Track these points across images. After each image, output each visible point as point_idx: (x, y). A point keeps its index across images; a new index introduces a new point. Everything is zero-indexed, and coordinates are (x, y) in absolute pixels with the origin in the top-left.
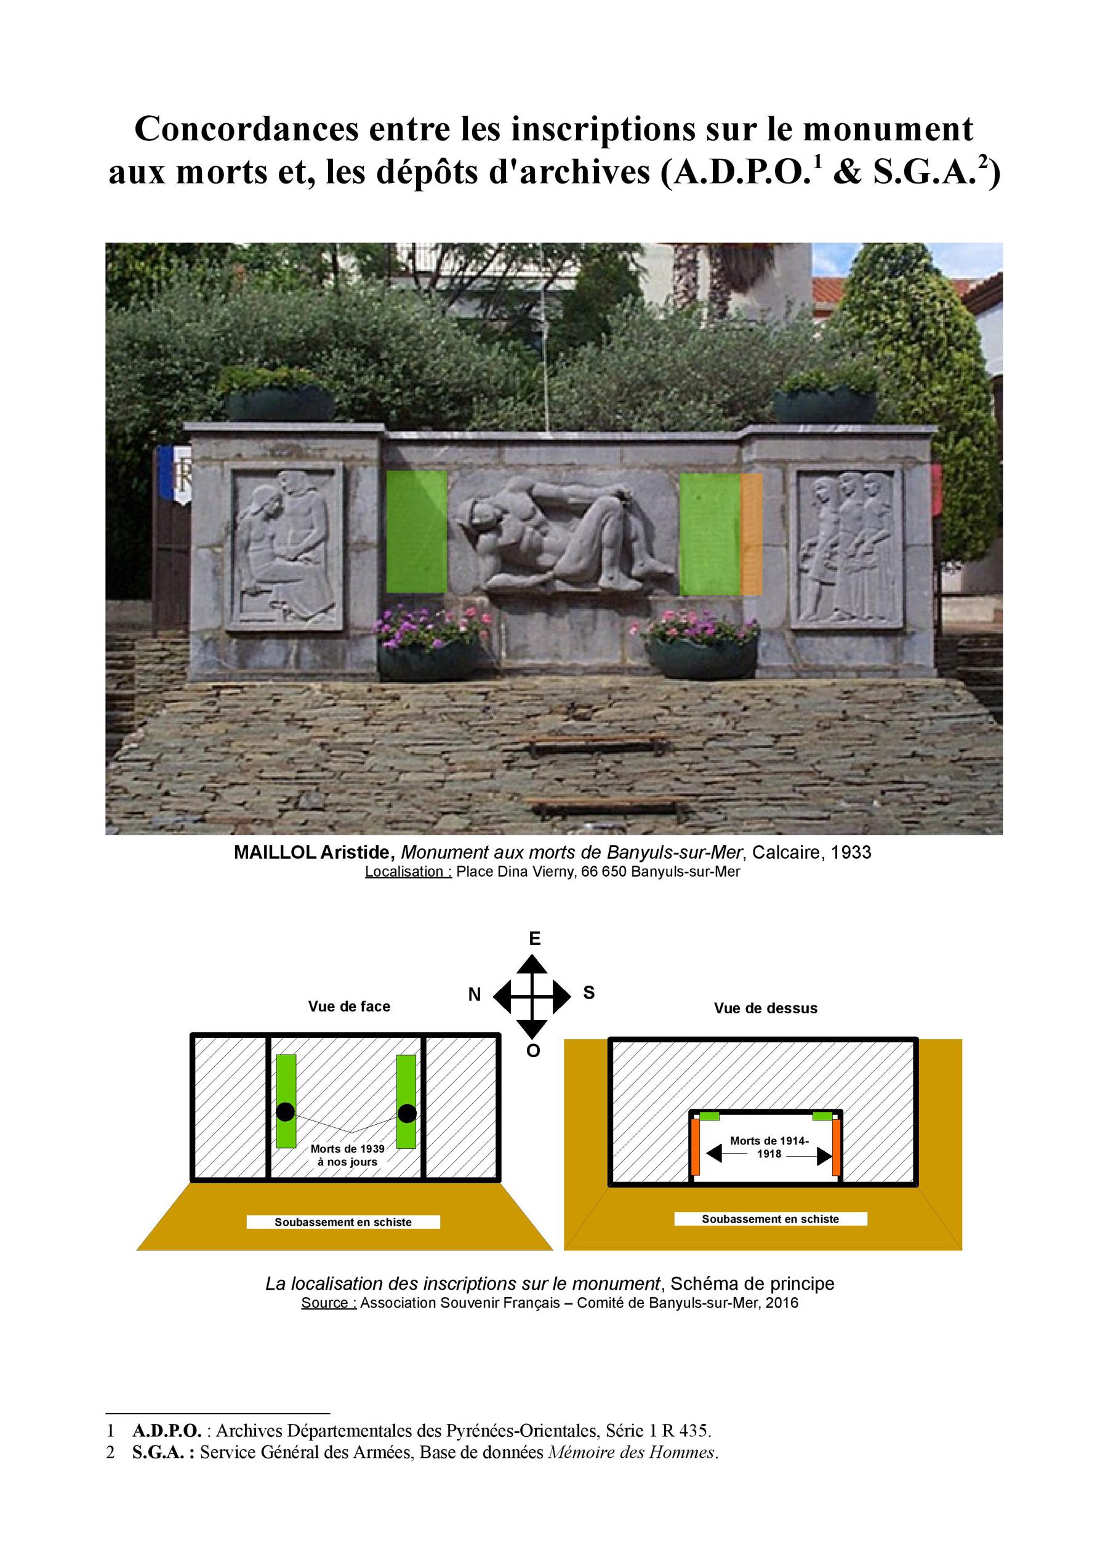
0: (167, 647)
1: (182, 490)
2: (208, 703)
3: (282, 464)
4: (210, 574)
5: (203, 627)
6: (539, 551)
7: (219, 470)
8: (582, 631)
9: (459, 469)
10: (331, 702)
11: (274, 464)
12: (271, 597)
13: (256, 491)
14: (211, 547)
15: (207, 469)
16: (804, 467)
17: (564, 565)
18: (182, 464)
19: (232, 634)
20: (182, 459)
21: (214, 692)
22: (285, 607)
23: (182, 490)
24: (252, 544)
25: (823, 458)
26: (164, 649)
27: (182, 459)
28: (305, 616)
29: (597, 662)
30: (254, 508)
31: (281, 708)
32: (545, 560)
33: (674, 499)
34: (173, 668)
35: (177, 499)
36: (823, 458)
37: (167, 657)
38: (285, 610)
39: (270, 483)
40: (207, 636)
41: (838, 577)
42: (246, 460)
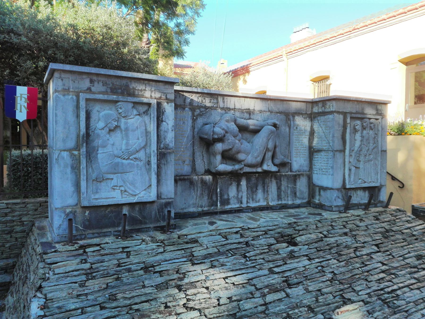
0: (9, 206)
1: (21, 112)
2: (81, 262)
3: (121, 98)
4: (69, 170)
5: (66, 204)
6: (239, 152)
7: (75, 97)
8: (252, 190)
9: (199, 109)
10: (161, 250)
11: (114, 97)
12: (114, 183)
13: (102, 114)
14: (70, 150)
15: (67, 97)
16: (354, 115)
17: (250, 159)
18: (21, 97)
19: (85, 208)
20: (21, 95)
21: (81, 251)
22: (123, 189)
23: (21, 112)
24: (100, 149)
25: (357, 112)
26: (8, 208)
27: (21, 95)
28: (134, 194)
29: (257, 204)
30: (101, 124)
31: (134, 259)
32: (241, 156)
33: (287, 130)
34: (15, 219)
35: (17, 118)
36: (357, 112)
37: (10, 212)
38: (121, 191)
39: (111, 109)
40: (68, 211)
41: (361, 165)
42: (94, 93)
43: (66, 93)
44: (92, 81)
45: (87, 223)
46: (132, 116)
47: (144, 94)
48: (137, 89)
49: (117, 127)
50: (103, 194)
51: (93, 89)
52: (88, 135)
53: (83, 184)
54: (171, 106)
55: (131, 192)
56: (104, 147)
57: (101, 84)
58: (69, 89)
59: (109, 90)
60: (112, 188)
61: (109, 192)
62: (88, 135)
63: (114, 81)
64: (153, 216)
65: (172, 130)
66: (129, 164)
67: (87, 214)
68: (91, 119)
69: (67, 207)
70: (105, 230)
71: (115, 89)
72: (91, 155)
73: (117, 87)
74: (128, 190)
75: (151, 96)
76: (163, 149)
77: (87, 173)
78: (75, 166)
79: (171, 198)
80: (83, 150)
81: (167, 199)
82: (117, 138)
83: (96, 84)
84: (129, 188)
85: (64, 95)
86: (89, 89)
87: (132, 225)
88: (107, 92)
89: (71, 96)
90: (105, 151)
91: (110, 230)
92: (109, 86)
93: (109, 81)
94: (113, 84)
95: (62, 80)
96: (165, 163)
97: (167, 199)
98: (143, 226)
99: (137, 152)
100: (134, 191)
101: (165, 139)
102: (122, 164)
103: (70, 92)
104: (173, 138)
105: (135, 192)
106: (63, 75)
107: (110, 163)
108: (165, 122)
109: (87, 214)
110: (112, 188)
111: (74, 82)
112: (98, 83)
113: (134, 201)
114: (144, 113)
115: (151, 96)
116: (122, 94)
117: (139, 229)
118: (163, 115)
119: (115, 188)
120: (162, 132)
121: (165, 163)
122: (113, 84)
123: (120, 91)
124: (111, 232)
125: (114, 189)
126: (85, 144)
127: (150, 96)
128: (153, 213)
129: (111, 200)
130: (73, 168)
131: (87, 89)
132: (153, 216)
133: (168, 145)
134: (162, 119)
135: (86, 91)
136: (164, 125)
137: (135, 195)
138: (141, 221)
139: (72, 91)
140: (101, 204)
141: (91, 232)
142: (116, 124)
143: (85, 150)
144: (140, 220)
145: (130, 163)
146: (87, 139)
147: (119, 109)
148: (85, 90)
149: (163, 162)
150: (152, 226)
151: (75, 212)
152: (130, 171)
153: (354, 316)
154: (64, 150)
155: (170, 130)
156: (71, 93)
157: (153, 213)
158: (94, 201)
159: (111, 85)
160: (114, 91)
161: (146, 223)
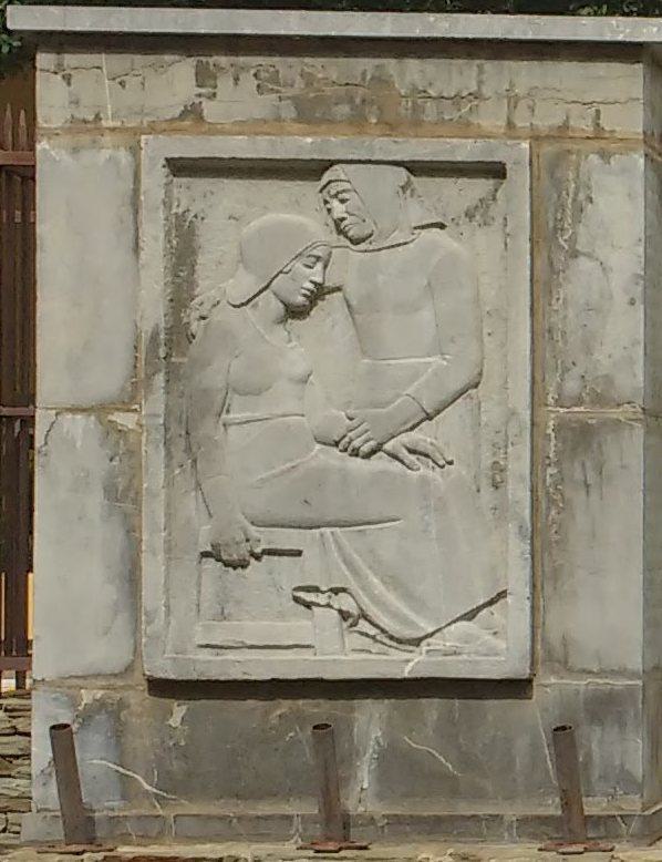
3: (335, 144)
4: (95, 501)
7: (124, 157)
11: (303, 145)
14: (100, 409)
15: (87, 156)
24: (235, 400)
30: (242, 284)
39: (296, 206)
40: (87, 697)
42: (214, 130)
43: (86, 139)
44: (203, 77)
45: (176, 766)
46: (398, 237)
47: (474, 120)
48: (432, 92)
49: (319, 293)
50: (252, 628)
51: (210, 110)
52: (177, 335)
53: (153, 570)
54: (624, 170)
55: (385, 622)
56: (254, 391)
57: (249, 82)
58: (98, 118)
59: (289, 112)
60: (296, 600)
61: (281, 616)
62: (177, 335)
63: (318, 66)
64: (520, 761)
65: (632, 302)
66: (379, 478)
67: (175, 721)
68: (201, 260)
69: (84, 677)
70: (264, 809)
71: (320, 100)
72: (188, 435)
73: (329, 91)
74: (373, 611)
75: (510, 124)
76: (579, 401)
77: (168, 515)
78: (121, 482)
79: (622, 673)
80: (155, 402)
81: (601, 673)
82: (316, 349)
83: (224, 85)
84: (376, 600)
85: (75, 150)
86: (193, 112)
87: (406, 795)
88: (278, 119)
89: (106, 154)
90: (257, 415)
91: (287, 809)
92: (290, 92)
93: (289, 67)
94: (309, 80)
95: (68, 79)
96: (592, 478)
97: (601, 673)
98: (464, 809)
99: (429, 417)
100: (412, 624)
101: (588, 351)
102: (345, 476)
103: (101, 131)
104: (635, 343)
105: (418, 628)
106: (70, 59)
107: (283, 473)
108: (589, 256)
109: (175, 721)
110: (296, 600)
111: (122, 84)
112: (236, 79)
113: (406, 672)
114: (470, 215)
115: (510, 124)
116: (357, 122)
117: (438, 820)
118: (577, 220)
119: (310, 597)
120: (571, 313)
121: (592, 478)
122: (309, 80)
123: (344, 109)
124: (289, 818)
125: (308, 605)
126: (160, 379)
127: (502, 123)
128: (522, 744)
129: (289, 655)
130: (112, 493)
131: (183, 115)
132: (520, 761)
133: (609, 380)
134: (573, 240)
135: (177, 124)
136: (581, 281)
137: (417, 642)
138: (454, 777)
139: (113, 129)
140: (236, 674)
141: (195, 809)
142: (318, 279)
143: (161, 409)
144: (447, 777)
145: (384, 472)
146: (172, 347)
147: (335, 203)
148: (172, 120)
149: (578, 475)
150: (511, 812)
151: (122, 705)
152: (392, 514)
153: (480, 813)
154: (74, 410)
155: (620, 299)
156: (107, 139)
157: (522, 744)
158: (205, 655)
159: (299, 83)
160: (310, 113)
161: (479, 795)
